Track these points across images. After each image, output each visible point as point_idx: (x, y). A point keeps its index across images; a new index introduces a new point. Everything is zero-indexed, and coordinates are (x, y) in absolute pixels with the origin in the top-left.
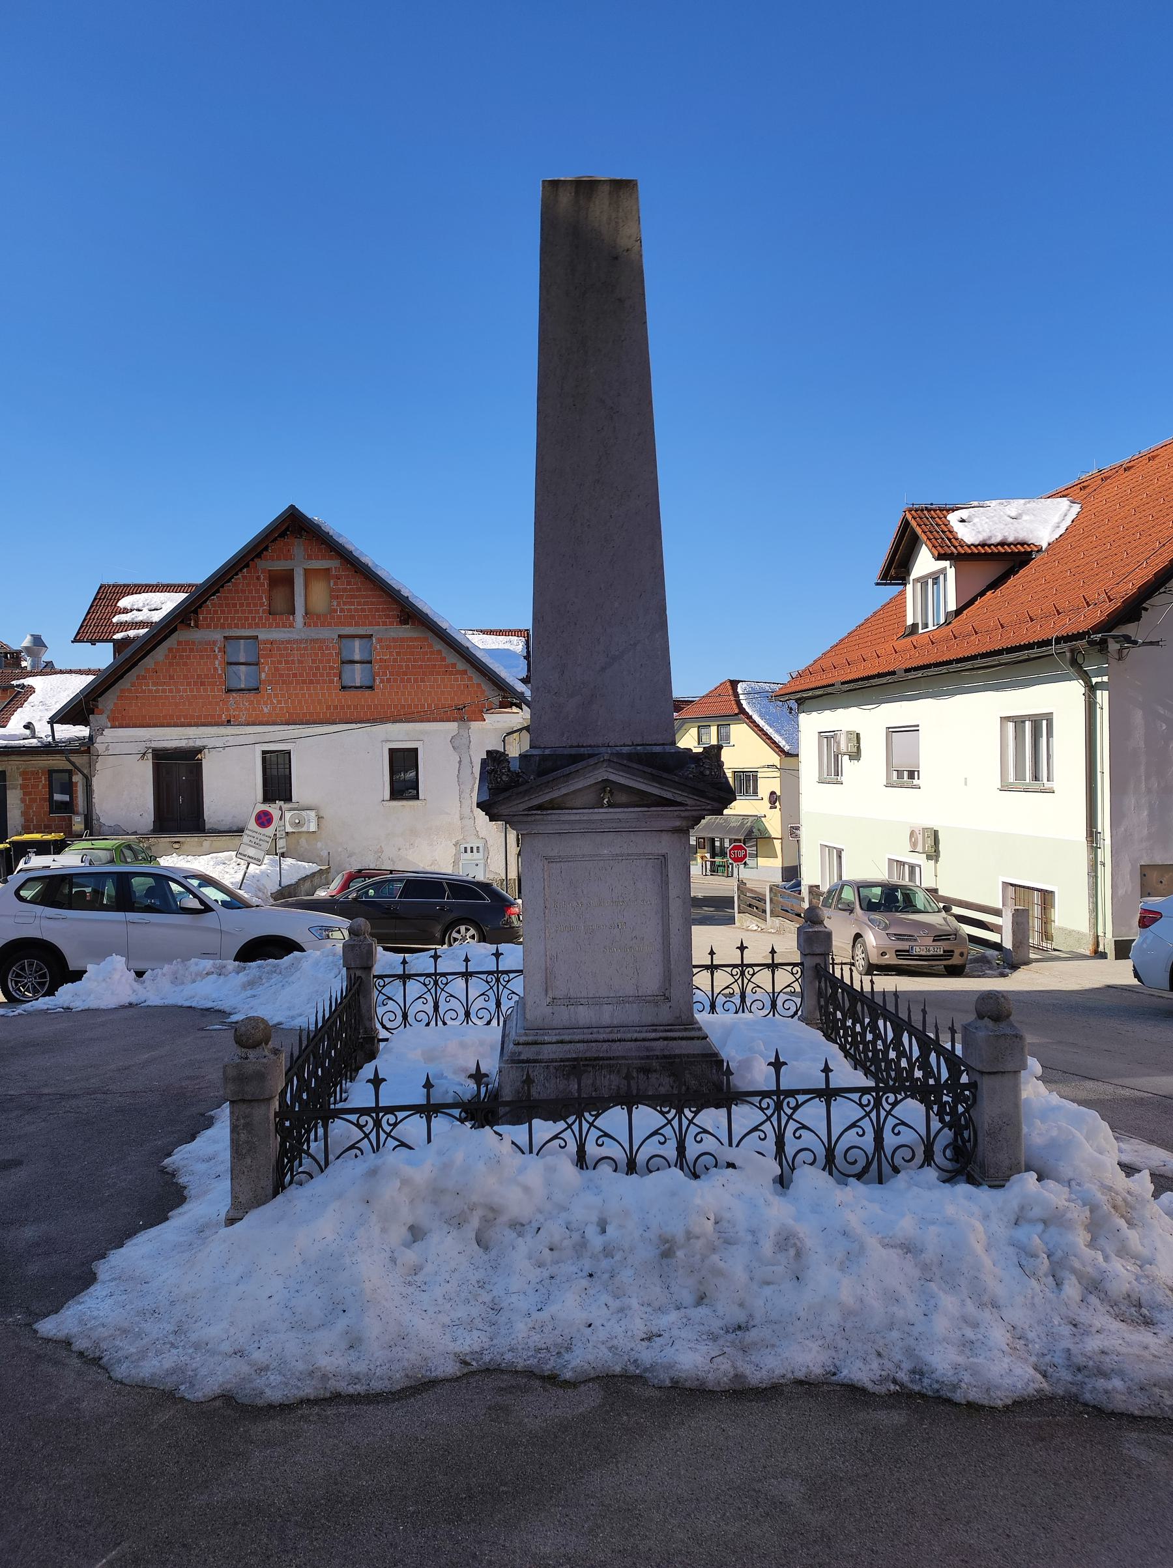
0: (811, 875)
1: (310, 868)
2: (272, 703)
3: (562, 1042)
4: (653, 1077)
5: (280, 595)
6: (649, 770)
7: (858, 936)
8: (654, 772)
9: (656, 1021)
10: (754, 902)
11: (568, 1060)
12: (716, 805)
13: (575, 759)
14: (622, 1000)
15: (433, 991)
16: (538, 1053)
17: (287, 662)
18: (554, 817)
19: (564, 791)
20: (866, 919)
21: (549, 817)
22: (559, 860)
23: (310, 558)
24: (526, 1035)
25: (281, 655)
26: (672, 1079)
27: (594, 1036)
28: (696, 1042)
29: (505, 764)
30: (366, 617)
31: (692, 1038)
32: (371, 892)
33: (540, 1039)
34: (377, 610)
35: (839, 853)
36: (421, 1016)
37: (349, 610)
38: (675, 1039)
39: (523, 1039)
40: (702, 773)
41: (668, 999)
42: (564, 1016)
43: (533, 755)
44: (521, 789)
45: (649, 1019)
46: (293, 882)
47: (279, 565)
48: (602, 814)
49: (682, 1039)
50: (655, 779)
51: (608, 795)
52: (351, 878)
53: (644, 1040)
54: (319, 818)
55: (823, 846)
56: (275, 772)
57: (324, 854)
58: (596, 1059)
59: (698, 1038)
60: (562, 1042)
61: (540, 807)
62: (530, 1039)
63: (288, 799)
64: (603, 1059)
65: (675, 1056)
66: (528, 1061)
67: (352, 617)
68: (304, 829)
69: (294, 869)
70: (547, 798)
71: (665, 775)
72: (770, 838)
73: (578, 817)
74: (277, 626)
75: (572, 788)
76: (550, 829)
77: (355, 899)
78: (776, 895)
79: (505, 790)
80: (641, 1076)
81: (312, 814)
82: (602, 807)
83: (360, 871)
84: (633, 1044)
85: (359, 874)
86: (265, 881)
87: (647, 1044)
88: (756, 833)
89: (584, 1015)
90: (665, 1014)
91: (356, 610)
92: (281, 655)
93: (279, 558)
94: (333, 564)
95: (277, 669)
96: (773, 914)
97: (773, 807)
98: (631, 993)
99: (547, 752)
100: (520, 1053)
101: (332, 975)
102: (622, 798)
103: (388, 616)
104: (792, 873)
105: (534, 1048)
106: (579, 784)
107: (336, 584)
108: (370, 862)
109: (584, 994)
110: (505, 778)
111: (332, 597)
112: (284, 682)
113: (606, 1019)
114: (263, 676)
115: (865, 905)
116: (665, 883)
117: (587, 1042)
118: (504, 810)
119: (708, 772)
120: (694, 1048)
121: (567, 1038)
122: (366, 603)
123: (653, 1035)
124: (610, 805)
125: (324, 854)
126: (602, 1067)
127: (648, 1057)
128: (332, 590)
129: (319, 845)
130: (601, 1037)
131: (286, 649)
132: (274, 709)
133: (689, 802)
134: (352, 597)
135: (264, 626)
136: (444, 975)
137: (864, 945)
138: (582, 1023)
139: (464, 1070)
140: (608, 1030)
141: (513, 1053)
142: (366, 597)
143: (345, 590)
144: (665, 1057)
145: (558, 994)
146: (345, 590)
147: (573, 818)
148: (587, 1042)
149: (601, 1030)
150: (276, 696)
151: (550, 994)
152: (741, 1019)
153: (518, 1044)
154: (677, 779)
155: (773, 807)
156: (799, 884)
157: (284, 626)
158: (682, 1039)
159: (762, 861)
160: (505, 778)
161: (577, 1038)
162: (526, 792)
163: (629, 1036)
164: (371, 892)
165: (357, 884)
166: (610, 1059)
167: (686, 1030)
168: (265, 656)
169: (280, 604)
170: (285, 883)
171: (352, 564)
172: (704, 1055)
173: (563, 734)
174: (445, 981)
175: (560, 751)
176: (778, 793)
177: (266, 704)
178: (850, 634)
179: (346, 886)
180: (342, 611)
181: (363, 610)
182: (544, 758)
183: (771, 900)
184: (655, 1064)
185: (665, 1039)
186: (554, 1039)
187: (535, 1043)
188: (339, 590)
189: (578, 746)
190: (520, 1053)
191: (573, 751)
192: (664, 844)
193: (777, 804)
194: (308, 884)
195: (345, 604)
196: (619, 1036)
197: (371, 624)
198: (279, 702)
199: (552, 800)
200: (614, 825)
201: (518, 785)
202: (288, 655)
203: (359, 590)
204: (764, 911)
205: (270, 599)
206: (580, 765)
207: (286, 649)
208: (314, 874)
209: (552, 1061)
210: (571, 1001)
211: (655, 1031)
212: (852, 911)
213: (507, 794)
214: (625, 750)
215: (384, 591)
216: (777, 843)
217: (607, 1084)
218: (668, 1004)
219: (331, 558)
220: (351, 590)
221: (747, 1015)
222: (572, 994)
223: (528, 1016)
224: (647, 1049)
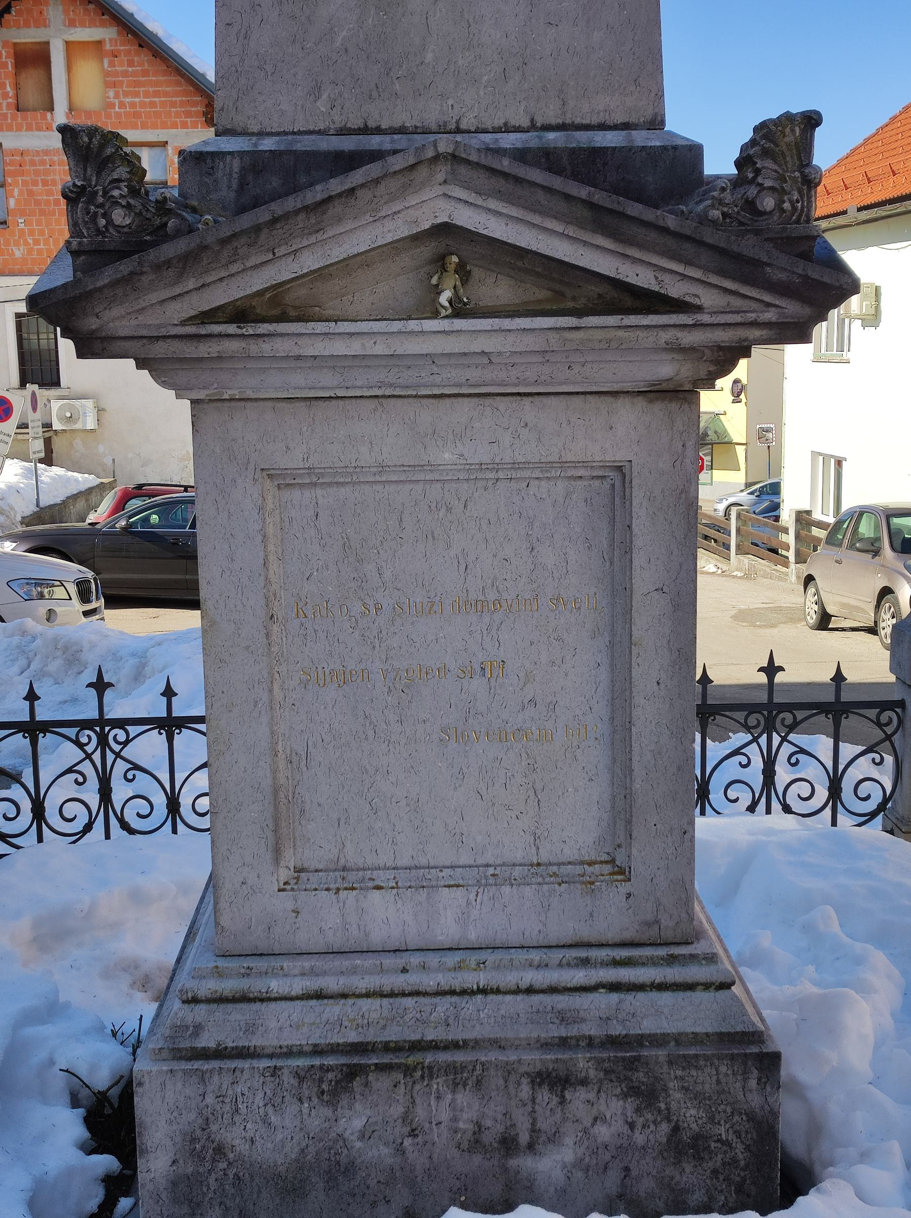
0: (795, 497)
1: (84, 480)
2: (26, 243)
3: (319, 996)
4: (578, 1098)
5: (31, 79)
6: (583, 192)
7: (886, 592)
8: (600, 197)
9: (586, 933)
10: (712, 533)
11: (335, 1049)
12: (792, 308)
13: (347, 162)
14: (491, 876)
15: (97, 757)
16: (250, 1029)
17: (45, 183)
18: (282, 347)
19: (310, 261)
20: (900, 566)
21: (266, 347)
22: (312, 478)
23: (72, 24)
24: (218, 973)
25: (37, 173)
26: (630, 1104)
27: (413, 980)
28: (699, 996)
29: (121, 172)
30: (157, 115)
31: (690, 987)
32: (155, 518)
33: (257, 986)
34: (173, 104)
35: (839, 463)
36: (72, 809)
37: (133, 105)
38: (640, 988)
39: (208, 987)
40: (750, 205)
41: (622, 873)
42: (327, 918)
43: (221, 155)
44: (169, 250)
45: (564, 926)
46: (58, 500)
47: (28, 36)
48: (437, 336)
49: (661, 987)
50: (602, 221)
51: (451, 280)
52: (126, 497)
53: (553, 990)
54: (100, 410)
55: (815, 454)
56: (34, 346)
57: (108, 461)
58: (417, 1046)
59: (707, 986)
60: (319, 996)
61: (240, 314)
62: (229, 986)
63: (56, 383)
64: (434, 1046)
65: (640, 1040)
66: (219, 1053)
67: (137, 115)
68: (78, 426)
69: (59, 481)
70: (258, 281)
71: (634, 209)
72: (730, 443)
73: (355, 347)
74: (30, 128)
75: (338, 253)
76: (274, 384)
77: (124, 529)
78: (745, 523)
79: (121, 255)
80: (544, 1095)
81: (89, 404)
82: (435, 315)
83: (140, 487)
84: (520, 1003)
85: (140, 491)
86: (14, 501)
87: (562, 1001)
88: (712, 436)
89: (385, 916)
90: (612, 914)
91: (143, 105)
92: (37, 173)
93: (27, 25)
94: (105, 33)
95: (31, 193)
96: (740, 550)
97: (737, 401)
98: (519, 856)
99: (268, 144)
100: (198, 1029)
101: (16, 669)
102: (495, 288)
103: (188, 114)
104: (769, 494)
105: (239, 1014)
106: (357, 235)
107: (111, 64)
108: (151, 476)
109: (386, 858)
110: (119, 217)
111: (108, 85)
112: (42, 213)
113: (447, 929)
114: (12, 203)
115: (898, 543)
116: (621, 547)
117: (392, 995)
118: (117, 319)
119: (769, 203)
120: (693, 1015)
121: (332, 984)
122: (157, 94)
123: (579, 977)
124: (459, 310)
125: (108, 461)
126: (430, 1072)
127: (564, 1043)
128: (107, 74)
129: (101, 449)
130: (430, 982)
131: (43, 163)
132: (30, 251)
133: (708, 298)
134: (137, 84)
135: (10, 129)
136: (121, 723)
137: (896, 604)
138: (378, 936)
139: (130, 966)
140: (452, 959)
141: (179, 1029)
142: (157, 84)
143: (125, 74)
144: (612, 1042)
145: (313, 857)
146: (125, 74)
147: (339, 348)
148: (392, 995)
149: (433, 960)
150: (32, 233)
151: (290, 859)
152: (770, 832)
153: (195, 1000)
154: (671, 222)
155: (737, 401)
156: (776, 507)
157: (39, 129)
158: (661, 987)
159: (719, 475)
160: (119, 217)
161: (362, 984)
162: (188, 262)
163: (510, 979)
164: (155, 518)
165: (134, 504)
166: (455, 1045)
167: (672, 960)
168: (14, 174)
169: (31, 95)
170: (45, 501)
171: (135, 34)
172: (725, 1038)
173: (316, 91)
174: (122, 737)
175: (305, 144)
176: (744, 381)
177: (17, 244)
178: (840, 161)
179: (120, 506)
180: (122, 105)
181: (152, 104)
182: (256, 164)
183: (738, 531)
184: (582, 1062)
185: (614, 987)
186: (298, 986)
187: (244, 998)
188: (116, 74)
189: (365, 130)
190: (198, 1029)
191: (348, 144)
192: (621, 434)
193: (742, 396)
194: (81, 504)
195: (126, 94)
196: (482, 979)
197: (164, 126)
198: (37, 242)
199: (277, 291)
200: (474, 375)
201: (161, 236)
202: (47, 173)
203: (145, 73)
204: (728, 548)
205: (17, 87)
206: (357, 177)
207: (43, 163)
208: (90, 491)
209: (290, 1053)
210: (349, 878)
211: (585, 962)
212: (876, 553)
213: (124, 267)
214: (509, 141)
215: (182, 75)
216: (740, 451)
217: (444, 1115)
218: (624, 888)
219: (103, 25)
220: (134, 74)
221: (779, 820)
222: (351, 856)
223: (225, 920)
224: (563, 1018)
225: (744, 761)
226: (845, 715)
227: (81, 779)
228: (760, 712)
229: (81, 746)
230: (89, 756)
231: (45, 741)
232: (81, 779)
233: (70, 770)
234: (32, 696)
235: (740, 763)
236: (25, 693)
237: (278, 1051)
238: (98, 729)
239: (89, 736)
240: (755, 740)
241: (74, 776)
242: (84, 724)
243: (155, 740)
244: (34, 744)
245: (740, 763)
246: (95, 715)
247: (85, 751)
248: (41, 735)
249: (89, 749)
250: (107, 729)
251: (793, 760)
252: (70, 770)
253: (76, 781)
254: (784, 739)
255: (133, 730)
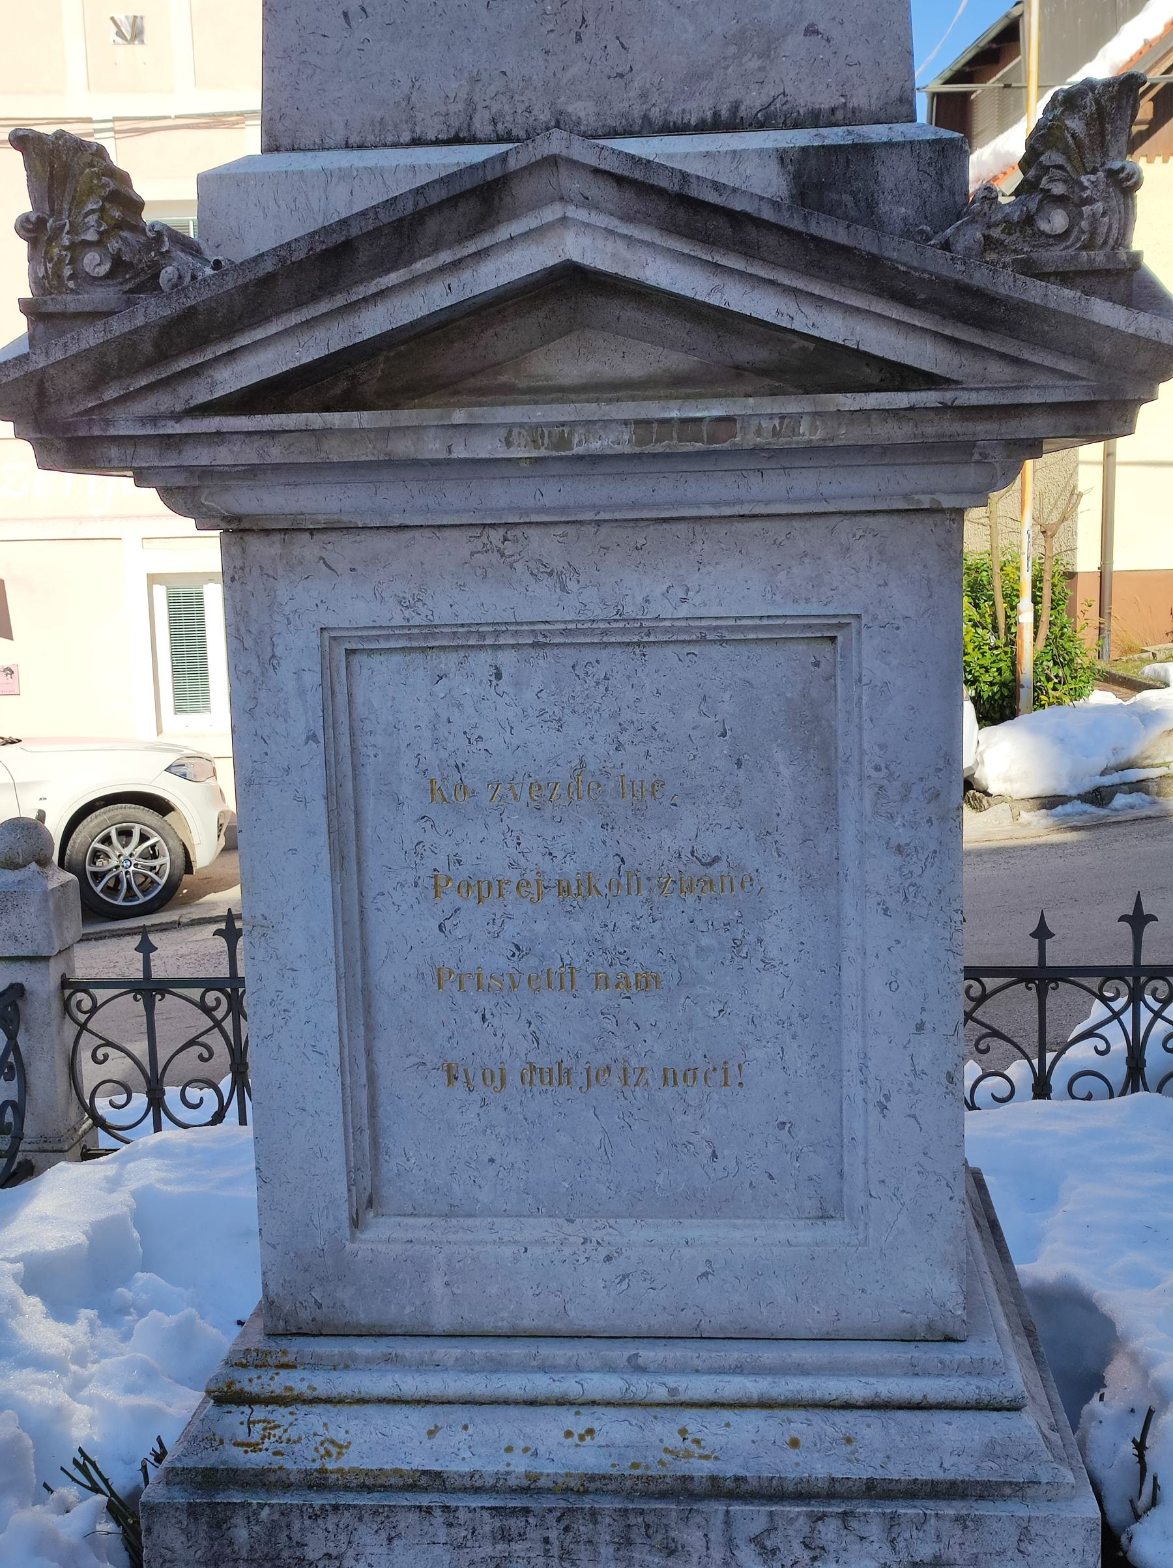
136: (85, 986)
225: (1102, 1046)
226: (1053, 985)
227: (206, 1055)
228: (1121, 979)
229: (208, 1011)
230: (218, 1024)
231: (1061, 996)
232: (206, 1055)
233: (193, 1042)
234: (1042, 933)
235: (1096, 1049)
236: (1033, 927)
237: (468, 1484)
238: (1130, 979)
239: (218, 1000)
240: (1116, 1015)
241: (196, 1050)
242: (209, 984)
243: (1023, 998)
244: (150, 1008)
245: (1096, 1049)
246: (1129, 961)
247: (213, 1018)
248: (158, 997)
249: (219, 1014)
250: (1143, 979)
251: (982, 1046)
252: (193, 1042)
253: (201, 1057)
254: (1157, 1015)
255: (102, 995)
